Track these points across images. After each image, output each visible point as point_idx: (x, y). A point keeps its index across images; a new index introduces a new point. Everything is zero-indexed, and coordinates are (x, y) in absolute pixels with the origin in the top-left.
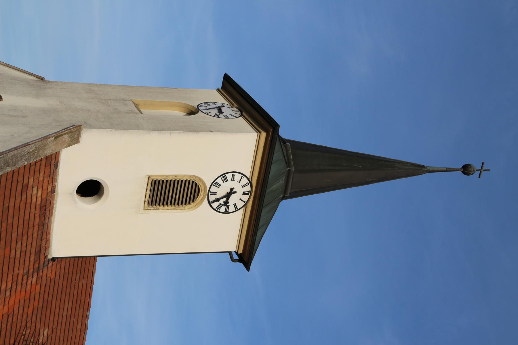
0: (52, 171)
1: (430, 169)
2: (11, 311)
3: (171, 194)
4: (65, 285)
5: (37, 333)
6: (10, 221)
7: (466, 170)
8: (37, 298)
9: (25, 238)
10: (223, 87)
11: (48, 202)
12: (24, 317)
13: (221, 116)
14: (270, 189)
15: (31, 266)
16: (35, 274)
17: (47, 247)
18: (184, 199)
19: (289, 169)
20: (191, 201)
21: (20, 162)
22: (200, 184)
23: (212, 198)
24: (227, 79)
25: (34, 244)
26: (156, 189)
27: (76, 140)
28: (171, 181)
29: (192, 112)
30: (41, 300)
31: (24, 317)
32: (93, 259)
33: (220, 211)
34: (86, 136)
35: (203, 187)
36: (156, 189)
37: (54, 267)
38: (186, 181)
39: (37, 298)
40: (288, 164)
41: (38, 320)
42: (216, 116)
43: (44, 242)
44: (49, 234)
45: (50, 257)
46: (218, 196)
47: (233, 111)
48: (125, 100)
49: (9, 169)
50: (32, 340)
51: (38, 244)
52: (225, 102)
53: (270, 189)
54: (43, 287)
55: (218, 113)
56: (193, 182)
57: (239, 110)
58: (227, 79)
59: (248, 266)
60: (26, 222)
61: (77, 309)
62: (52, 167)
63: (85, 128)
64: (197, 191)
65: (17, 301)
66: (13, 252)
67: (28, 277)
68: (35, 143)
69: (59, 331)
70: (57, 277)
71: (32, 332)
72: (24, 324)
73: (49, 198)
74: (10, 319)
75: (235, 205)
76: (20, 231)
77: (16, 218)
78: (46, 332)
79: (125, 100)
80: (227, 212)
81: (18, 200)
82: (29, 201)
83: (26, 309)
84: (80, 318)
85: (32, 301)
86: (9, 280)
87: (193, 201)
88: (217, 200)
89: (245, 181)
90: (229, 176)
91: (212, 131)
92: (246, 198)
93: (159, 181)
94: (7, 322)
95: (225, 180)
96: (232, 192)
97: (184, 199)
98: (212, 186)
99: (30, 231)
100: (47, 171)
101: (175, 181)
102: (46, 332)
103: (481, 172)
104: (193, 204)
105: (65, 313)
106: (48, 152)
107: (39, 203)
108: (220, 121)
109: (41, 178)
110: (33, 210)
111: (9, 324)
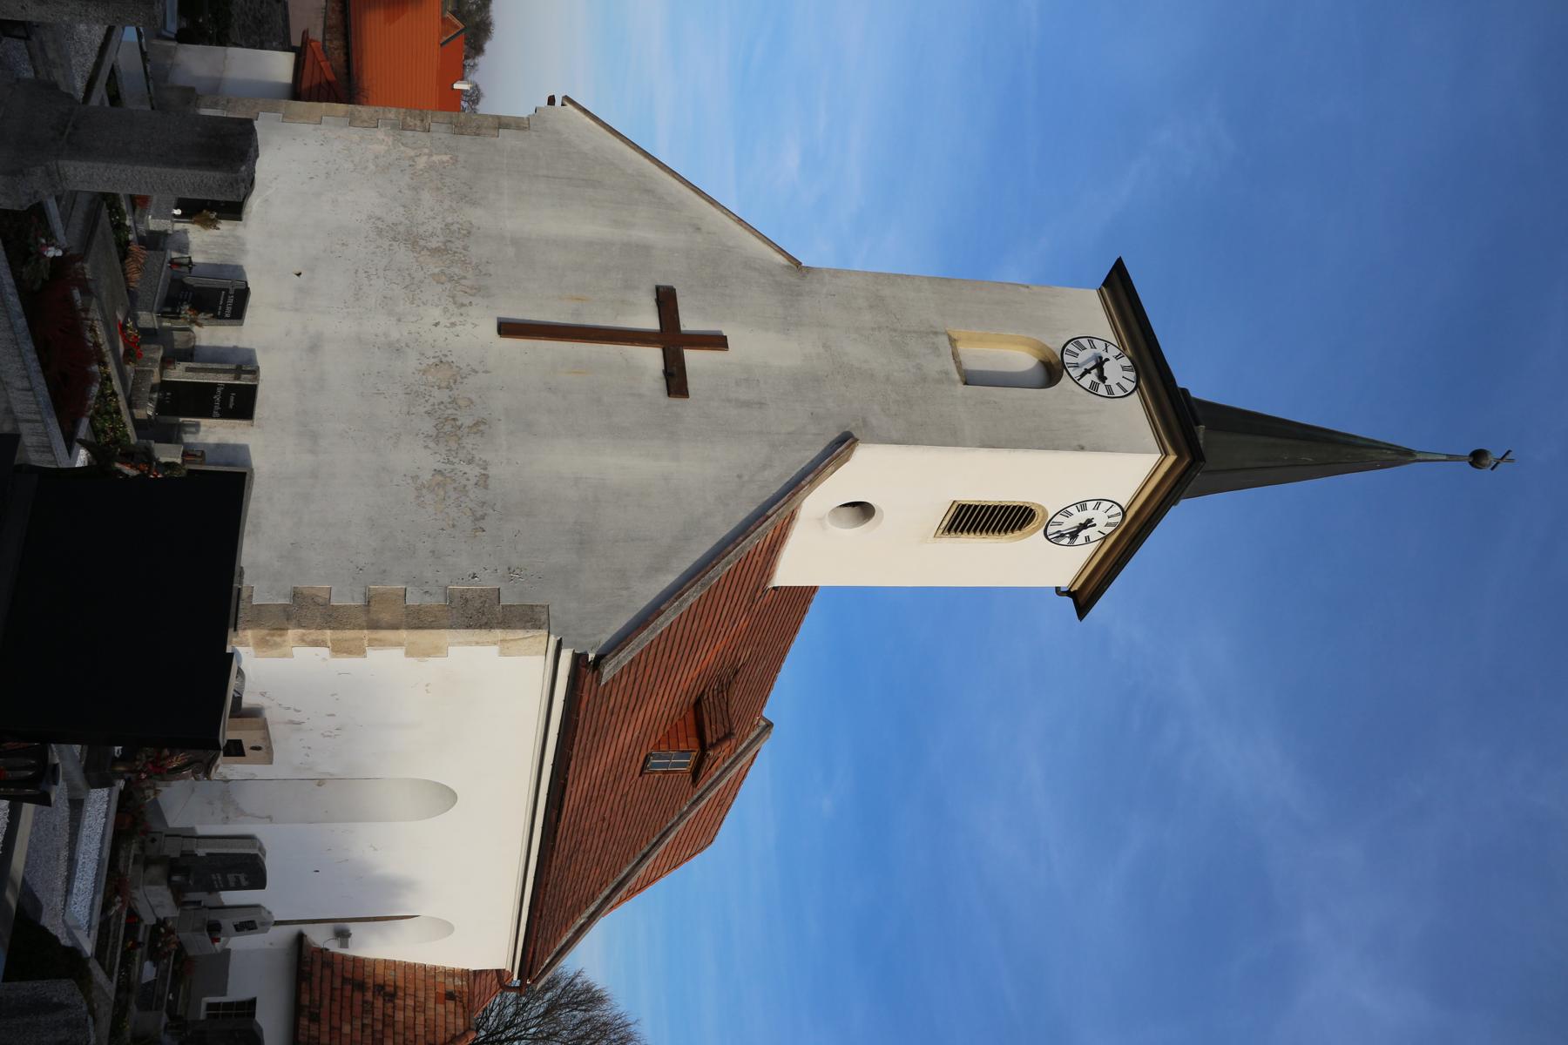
7: (1477, 458)
17: (769, 576)
22: (1039, 512)
35: (1041, 515)
42: (1093, 389)
52: (1112, 338)
58: (1119, 263)
79: (936, 333)
87: (1020, 529)
89: (1117, 510)
90: (1091, 505)
91: (1082, 448)
92: (1108, 530)
104: (1017, 533)
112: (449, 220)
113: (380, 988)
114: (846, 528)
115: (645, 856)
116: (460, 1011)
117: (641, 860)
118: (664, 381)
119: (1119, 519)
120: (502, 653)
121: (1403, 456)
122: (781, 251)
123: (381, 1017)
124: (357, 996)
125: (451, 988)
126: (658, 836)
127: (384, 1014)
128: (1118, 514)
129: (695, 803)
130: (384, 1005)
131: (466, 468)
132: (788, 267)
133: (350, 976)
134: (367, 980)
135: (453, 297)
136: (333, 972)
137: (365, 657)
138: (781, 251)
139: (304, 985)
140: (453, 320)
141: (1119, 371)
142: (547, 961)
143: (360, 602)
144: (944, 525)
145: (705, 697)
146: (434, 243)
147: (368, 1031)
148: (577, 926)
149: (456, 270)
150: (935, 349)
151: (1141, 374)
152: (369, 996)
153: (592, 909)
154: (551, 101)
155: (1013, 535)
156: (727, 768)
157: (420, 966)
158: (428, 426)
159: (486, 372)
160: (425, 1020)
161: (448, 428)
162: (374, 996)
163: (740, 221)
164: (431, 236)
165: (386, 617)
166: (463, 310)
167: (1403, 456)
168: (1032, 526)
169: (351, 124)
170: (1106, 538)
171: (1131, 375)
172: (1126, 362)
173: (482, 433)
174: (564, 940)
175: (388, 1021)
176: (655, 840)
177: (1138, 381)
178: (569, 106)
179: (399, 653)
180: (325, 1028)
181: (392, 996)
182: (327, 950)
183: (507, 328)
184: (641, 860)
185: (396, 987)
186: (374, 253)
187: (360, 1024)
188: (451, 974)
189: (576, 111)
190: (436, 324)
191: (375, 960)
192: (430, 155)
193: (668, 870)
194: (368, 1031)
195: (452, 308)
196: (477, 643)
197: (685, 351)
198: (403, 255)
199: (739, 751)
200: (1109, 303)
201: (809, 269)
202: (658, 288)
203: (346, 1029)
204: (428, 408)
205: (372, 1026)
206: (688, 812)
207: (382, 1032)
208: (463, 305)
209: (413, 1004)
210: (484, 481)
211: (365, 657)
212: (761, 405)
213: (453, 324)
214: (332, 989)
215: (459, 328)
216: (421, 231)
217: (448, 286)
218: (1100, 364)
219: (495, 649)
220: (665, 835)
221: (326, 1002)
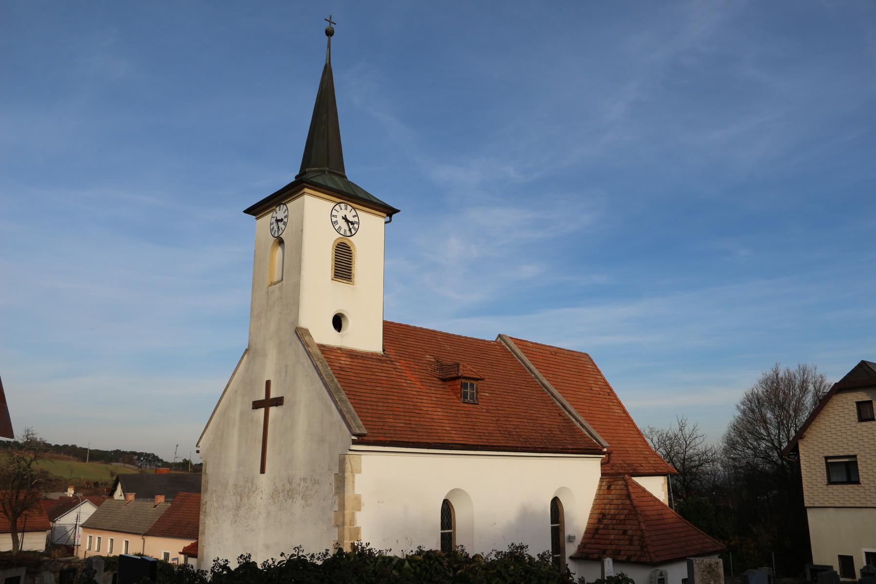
0: (327, 349)
1: (328, 61)
2: (419, 380)
3: (344, 264)
4: (397, 343)
5: (429, 363)
6: (364, 380)
7: (329, 33)
8: (409, 362)
9: (374, 370)
10: (254, 215)
11: (349, 353)
12: (420, 371)
13: (285, 220)
14: (343, 188)
15: (389, 366)
16: (394, 363)
17: (376, 354)
18: (348, 254)
19: (326, 172)
20: (349, 249)
21: (330, 373)
22: (339, 241)
23: (348, 234)
24: (248, 211)
25: (375, 363)
26: (340, 275)
27: (307, 332)
28: (335, 264)
29: (280, 242)
30: (409, 359)
31: (420, 371)
32: (384, 322)
33: (357, 228)
34: (304, 323)
35: (341, 240)
36: (340, 275)
37: (388, 350)
38: (336, 252)
39: (409, 362)
40: (323, 172)
41: (421, 361)
42: (285, 224)
43: (374, 357)
44: (367, 353)
45: (382, 353)
46: (347, 229)
47: (280, 210)
48: (268, 292)
49: (336, 380)
50: (434, 366)
51: (375, 360)
52: (270, 215)
53: (343, 188)
54: (401, 358)
55: (283, 222)
56: (336, 247)
57: (279, 205)
58: (248, 211)
59: (396, 211)
60: (363, 369)
61: (411, 334)
62: (325, 349)
63: (298, 325)
64: (342, 244)
65: (412, 376)
66: (383, 378)
67: (396, 368)
68: (577, 360)
69: (426, 348)
70: (393, 348)
71: (429, 366)
72: (425, 371)
73: (345, 352)
74: (423, 380)
75: (354, 216)
76: (369, 373)
77: (362, 376)
78: (427, 356)
79: (268, 292)
80: (358, 223)
81: (350, 374)
82: (349, 366)
83: (417, 370)
84: (416, 333)
85: (411, 366)
86: (400, 381)
87: (349, 248)
88: (350, 230)
89: (337, 207)
90: (334, 219)
91: (302, 230)
92: (349, 208)
93: (335, 272)
94: (425, 382)
95: (336, 222)
96: (345, 218)
97: (348, 254)
98: (340, 232)
99: (369, 366)
100: (328, 353)
101: (335, 261)
102: (427, 356)
103: (332, 22)
104: (352, 248)
105: (415, 343)
106: (319, 352)
107: (350, 360)
108: (291, 221)
109: (334, 357)
110: (355, 364)
111: (427, 381)
112: (232, 493)
113: (600, 521)
114: (348, 323)
115: (552, 395)
116: (616, 483)
117: (554, 396)
118: (279, 406)
119: (343, 205)
120: (360, 472)
121: (328, 72)
122: (243, 357)
123: (611, 521)
124: (600, 532)
125: (606, 487)
126: (544, 388)
127: (610, 519)
128: (340, 206)
129: (531, 371)
130: (607, 519)
131: (302, 486)
132: (248, 354)
133: (592, 535)
134: (595, 527)
135: (254, 491)
136: (588, 543)
137: (360, 527)
138: (243, 357)
139: (590, 557)
140: (260, 492)
141: (280, 213)
142: (595, 441)
143: (336, 529)
144: (347, 282)
145: (440, 377)
146: (239, 499)
147: (615, 527)
148: (581, 427)
149: (246, 490)
150: (273, 292)
151: (280, 202)
152: (601, 526)
153: (573, 420)
154: (198, 452)
155: (353, 250)
156: (517, 356)
157: (594, 502)
158: (289, 501)
159: (275, 478)
160: (616, 499)
161: (290, 494)
162: (602, 524)
163: (234, 374)
164: (236, 500)
165: (341, 519)
166: (258, 488)
167: (328, 72)
168: (349, 244)
169: (204, 534)
170: (354, 208)
171: (282, 206)
172: (278, 209)
173: (292, 480)
174: (586, 433)
175: (613, 517)
176: (546, 390)
177: (282, 204)
178: (200, 444)
179: (359, 516)
180: (609, 547)
181: (604, 515)
182: (579, 546)
183: (263, 471)
184: (555, 397)
185: (600, 514)
186: (241, 524)
187: (611, 530)
188: (600, 486)
189: (201, 442)
190: (262, 498)
191: (588, 523)
192: (213, 501)
193: (601, 375)
194: (615, 527)
195: (257, 492)
196: (353, 482)
197: (271, 398)
198: (242, 512)
199: (510, 350)
200: (295, 196)
201: (249, 345)
202: (253, 409)
203: (612, 537)
204: (284, 502)
205: (614, 525)
206: (534, 374)
207: (617, 520)
208: (256, 488)
209: (608, 505)
210: (305, 479)
211: (360, 527)
212: (286, 367)
213: (262, 492)
214: (595, 543)
215: (263, 490)
216: (235, 505)
217: (251, 493)
218: (278, 221)
219: (357, 476)
220: (544, 385)
221: (599, 546)
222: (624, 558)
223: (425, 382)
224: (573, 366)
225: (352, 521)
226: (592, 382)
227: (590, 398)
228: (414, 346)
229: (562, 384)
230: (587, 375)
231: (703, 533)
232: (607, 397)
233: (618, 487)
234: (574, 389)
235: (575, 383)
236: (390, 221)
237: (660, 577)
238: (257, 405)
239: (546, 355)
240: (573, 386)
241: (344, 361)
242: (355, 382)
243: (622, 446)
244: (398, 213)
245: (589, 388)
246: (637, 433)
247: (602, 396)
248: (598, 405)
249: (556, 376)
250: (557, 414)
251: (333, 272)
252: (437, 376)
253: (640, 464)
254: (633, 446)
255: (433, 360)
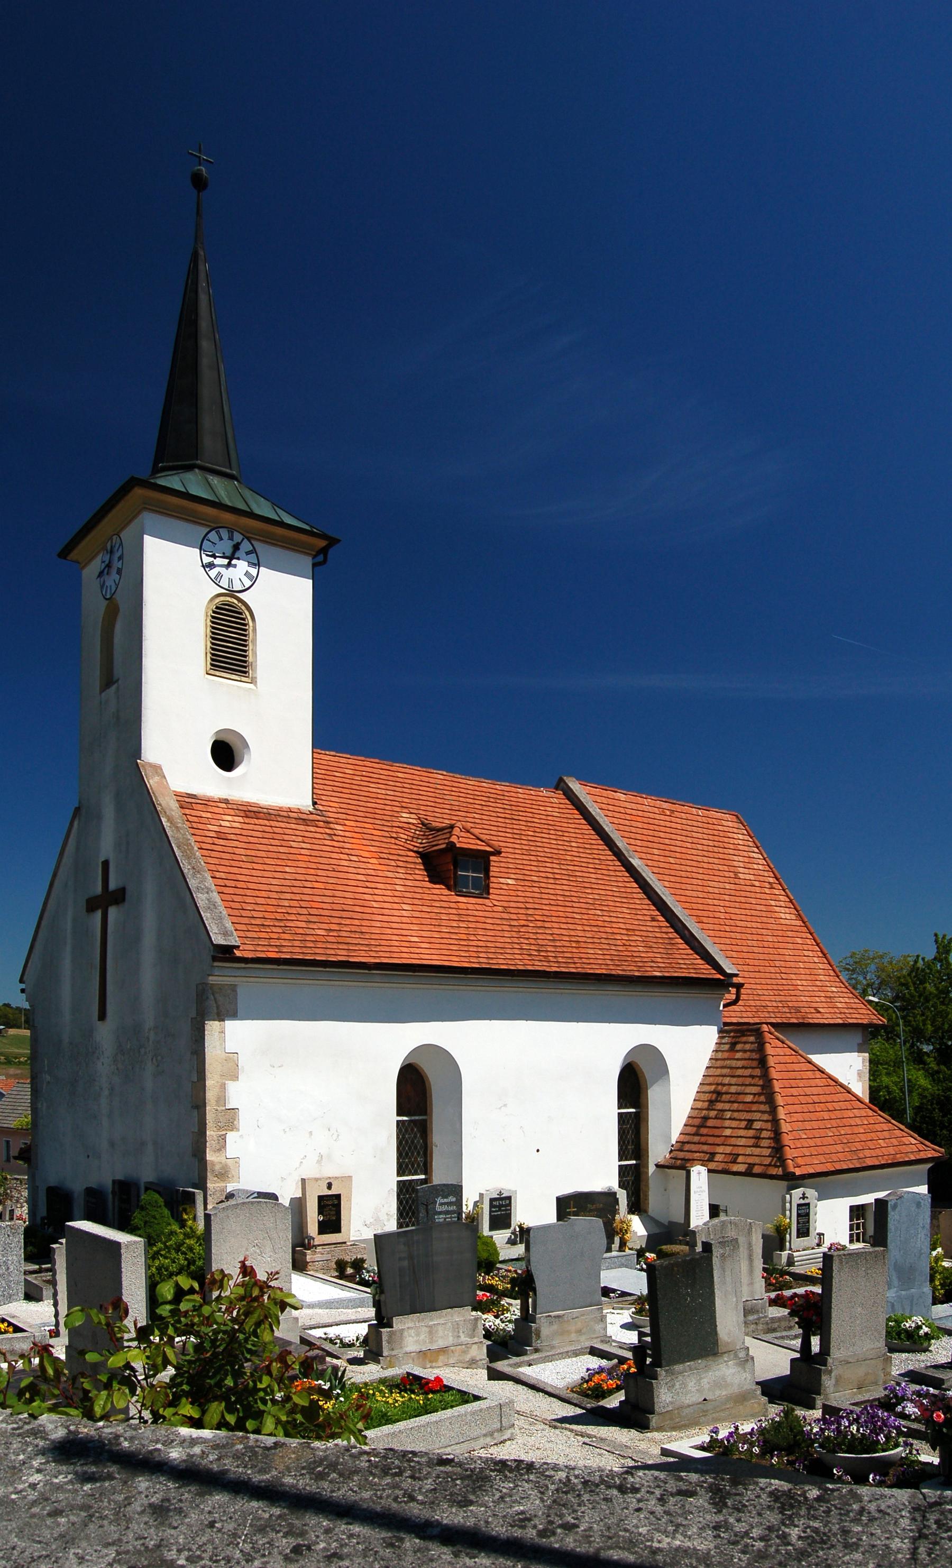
0: (200, 802)
16: (332, 826)
25: (293, 826)
43: (292, 815)
45: (311, 808)
48: (101, 703)
53: (226, 499)
67: (335, 835)
79: (101, 703)
94: (389, 859)
106: (174, 805)
128: (218, 533)
145: (421, 850)
152: (713, 1114)
178: (25, 978)
183: (102, 1016)
201: (80, 802)
222: (742, 1168)
223: (389, 859)
224: (705, 837)
225: (222, 1098)
226: (741, 864)
227: (733, 893)
228: (380, 796)
229: (677, 867)
230: (731, 852)
231: (902, 1127)
232: (767, 891)
233: (748, 1047)
234: (700, 876)
235: (705, 865)
236: (325, 561)
237: (802, 1201)
238: (92, 905)
239: (651, 815)
240: (701, 871)
241: (229, 822)
242: (244, 858)
243: (784, 976)
244: (338, 545)
245: (732, 875)
246: (821, 955)
247: (758, 890)
248: (747, 906)
249: (667, 853)
250: (648, 918)
251: (209, 661)
252: (415, 849)
253: (815, 1008)
254: (808, 977)
255: (414, 821)
